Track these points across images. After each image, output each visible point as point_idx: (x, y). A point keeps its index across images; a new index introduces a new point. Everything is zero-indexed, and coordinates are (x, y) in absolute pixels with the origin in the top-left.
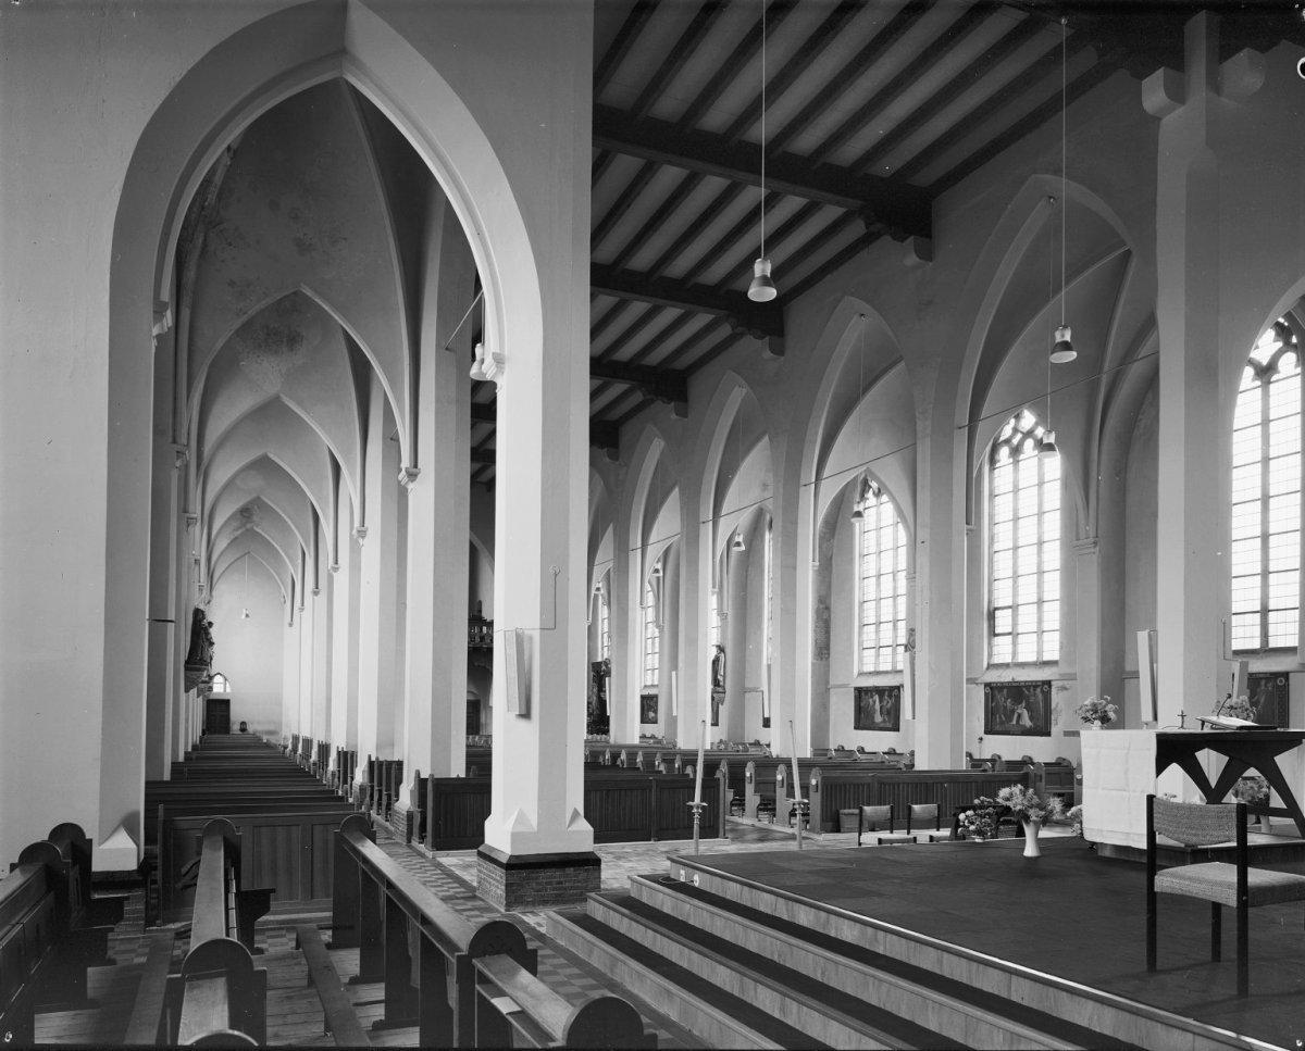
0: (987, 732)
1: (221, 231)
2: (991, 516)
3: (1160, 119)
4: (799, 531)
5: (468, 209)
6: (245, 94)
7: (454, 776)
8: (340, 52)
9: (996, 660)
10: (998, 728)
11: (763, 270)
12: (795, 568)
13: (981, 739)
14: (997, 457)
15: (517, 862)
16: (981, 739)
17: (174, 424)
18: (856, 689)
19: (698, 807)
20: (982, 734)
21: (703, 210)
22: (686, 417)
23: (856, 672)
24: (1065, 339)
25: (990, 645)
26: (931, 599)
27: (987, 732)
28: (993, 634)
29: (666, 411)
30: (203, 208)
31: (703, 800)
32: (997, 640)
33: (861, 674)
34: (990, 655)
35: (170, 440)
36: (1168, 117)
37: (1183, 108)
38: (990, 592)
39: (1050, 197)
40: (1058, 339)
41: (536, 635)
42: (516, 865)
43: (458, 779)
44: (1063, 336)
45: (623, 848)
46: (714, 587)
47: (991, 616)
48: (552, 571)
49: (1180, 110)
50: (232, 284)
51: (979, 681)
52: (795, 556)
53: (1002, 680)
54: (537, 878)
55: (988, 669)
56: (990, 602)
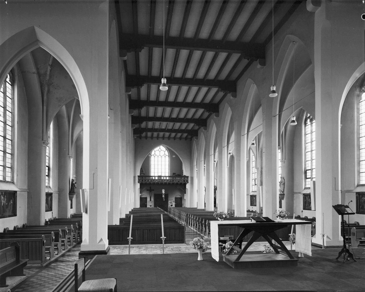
0: (304, 209)
1: (53, 86)
2: (305, 141)
3: (315, 12)
4: (241, 149)
5: (174, 66)
6: (11, 57)
7: (114, 224)
8: (37, 41)
9: (307, 186)
10: (306, 208)
11: (164, 82)
12: (240, 160)
13: (302, 211)
14: (307, 123)
15: (82, 253)
16: (302, 211)
17: (43, 136)
18: (357, 193)
19: (130, 239)
20: (302, 210)
21: (212, 58)
22: (219, 117)
23: (356, 184)
24: (274, 90)
25: (305, 181)
26: (266, 170)
27: (304, 209)
28: (306, 178)
29: (214, 116)
30: (46, 80)
31: (131, 237)
32: (307, 180)
33: (359, 185)
34: (305, 185)
35: (41, 139)
36: (317, 11)
37: (320, 8)
38: (305, 165)
39: (294, 42)
40: (272, 89)
41: (88, 190)
42: (82, 253)
43: (116, 225)
44: (273, 89)
45: (153, 246)
46: (227, 166)
47: (306, 173)
48: (92, 173)
49: (320, 9)
50: (57, 98)
51: (354, 191)
52: (240, 157)
53: (307, 193)
54: (88, 257)
55: (305, 189)
56: (305, 168)
